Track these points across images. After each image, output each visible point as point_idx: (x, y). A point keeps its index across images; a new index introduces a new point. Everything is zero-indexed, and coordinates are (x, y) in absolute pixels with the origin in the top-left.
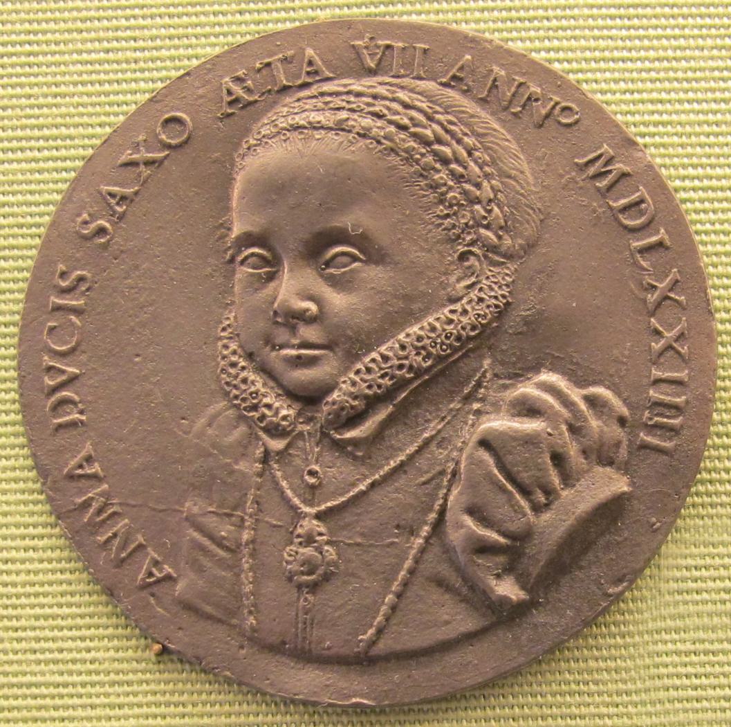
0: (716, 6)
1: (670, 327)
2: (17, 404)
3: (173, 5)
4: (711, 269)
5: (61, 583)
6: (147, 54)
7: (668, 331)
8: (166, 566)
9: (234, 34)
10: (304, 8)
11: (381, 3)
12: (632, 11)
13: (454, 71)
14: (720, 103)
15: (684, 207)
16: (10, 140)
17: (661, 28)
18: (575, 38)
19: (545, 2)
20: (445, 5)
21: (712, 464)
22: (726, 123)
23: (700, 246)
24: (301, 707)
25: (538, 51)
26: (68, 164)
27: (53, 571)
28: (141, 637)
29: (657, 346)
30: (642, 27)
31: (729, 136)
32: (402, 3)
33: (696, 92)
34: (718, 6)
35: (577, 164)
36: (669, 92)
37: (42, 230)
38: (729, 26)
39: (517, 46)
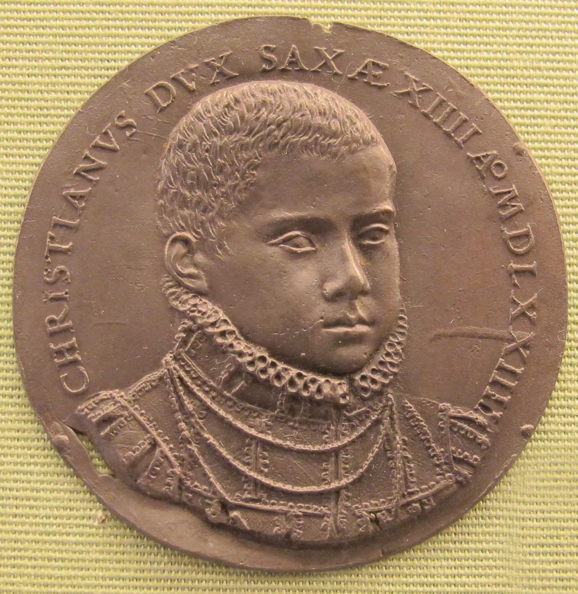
1: (526, 298)
2: (11, 280)
6: (58, 23)
7: (522, 301)
8: (461, 113)
12: (191, 9)
13: (359, 70)
14: (522, 39)
15: (554, 195)
20: (346, 4)
23: (558, 209)
24: (186, 558)
25: (452, 59)
26: (83, 88)
28: (74, 475)
29: (514, 312)
30: (530, 109)
33: (552, 62)
34: (103, 4)
35: (468, 157)
36: (538, 15)
37: (55, 135)
39: (438, 54)
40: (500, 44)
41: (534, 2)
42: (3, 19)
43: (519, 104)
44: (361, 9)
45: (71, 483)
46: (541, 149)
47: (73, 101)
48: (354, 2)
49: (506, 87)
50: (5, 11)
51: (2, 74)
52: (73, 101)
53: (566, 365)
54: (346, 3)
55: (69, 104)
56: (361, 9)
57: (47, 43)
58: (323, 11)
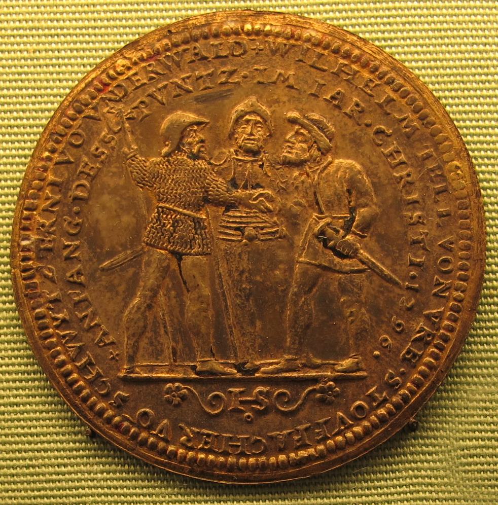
0: (114, 4)
2: (14, 304)
3: (323, 4)
4: (481, 176)
5: (83, 458)
9: (143, 27)
10: (293, 6)
11: (166, 2)
16: (5, 112)
17: (386, 17)
18: (390, 24)
19: (77, 1)
21: (484, 308)
22: (494, 158)
27: (57, 434)
31: (496, 91)
32: (206, 2)
38: (496, 15)
40: (448, 45)
41: (51, 2)
42: (3, 104)
43: (400, 12)
44: (101, 28)
45: (168, 487)
46: (430, 53)
47: (40, 119)
48: (442, 1)
49: (487, 123)
50: (5, 459)
51: (2, 498)
52: (40, 119)
53: (488, 288)
54: (255, 2)
55: (37, 122)
56: (101, 28)
57: (105, 34)
58: (112, 23)
